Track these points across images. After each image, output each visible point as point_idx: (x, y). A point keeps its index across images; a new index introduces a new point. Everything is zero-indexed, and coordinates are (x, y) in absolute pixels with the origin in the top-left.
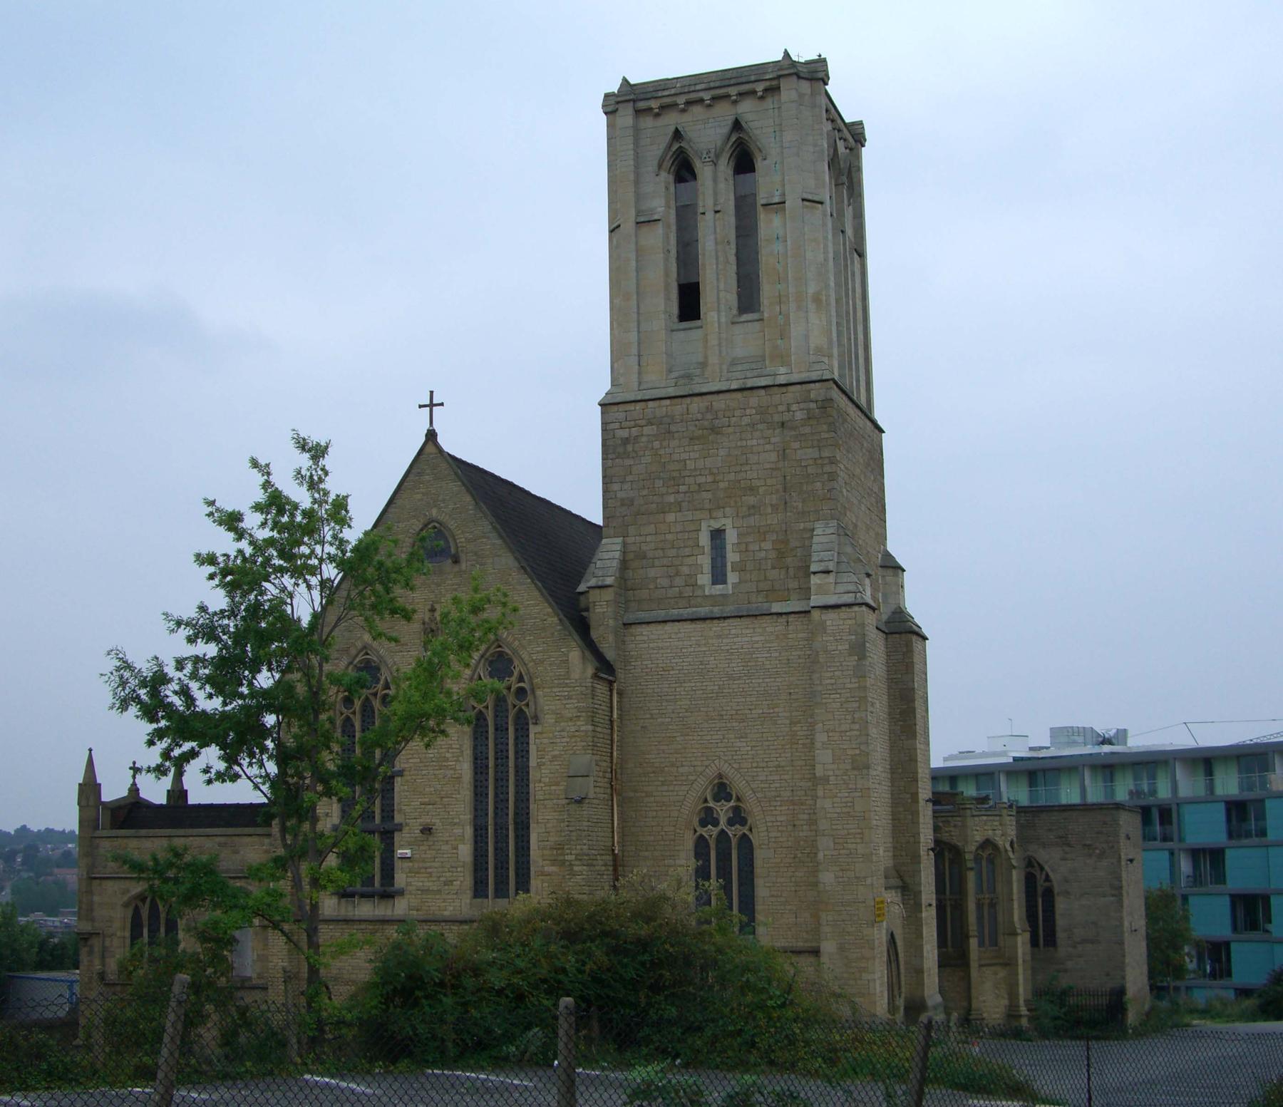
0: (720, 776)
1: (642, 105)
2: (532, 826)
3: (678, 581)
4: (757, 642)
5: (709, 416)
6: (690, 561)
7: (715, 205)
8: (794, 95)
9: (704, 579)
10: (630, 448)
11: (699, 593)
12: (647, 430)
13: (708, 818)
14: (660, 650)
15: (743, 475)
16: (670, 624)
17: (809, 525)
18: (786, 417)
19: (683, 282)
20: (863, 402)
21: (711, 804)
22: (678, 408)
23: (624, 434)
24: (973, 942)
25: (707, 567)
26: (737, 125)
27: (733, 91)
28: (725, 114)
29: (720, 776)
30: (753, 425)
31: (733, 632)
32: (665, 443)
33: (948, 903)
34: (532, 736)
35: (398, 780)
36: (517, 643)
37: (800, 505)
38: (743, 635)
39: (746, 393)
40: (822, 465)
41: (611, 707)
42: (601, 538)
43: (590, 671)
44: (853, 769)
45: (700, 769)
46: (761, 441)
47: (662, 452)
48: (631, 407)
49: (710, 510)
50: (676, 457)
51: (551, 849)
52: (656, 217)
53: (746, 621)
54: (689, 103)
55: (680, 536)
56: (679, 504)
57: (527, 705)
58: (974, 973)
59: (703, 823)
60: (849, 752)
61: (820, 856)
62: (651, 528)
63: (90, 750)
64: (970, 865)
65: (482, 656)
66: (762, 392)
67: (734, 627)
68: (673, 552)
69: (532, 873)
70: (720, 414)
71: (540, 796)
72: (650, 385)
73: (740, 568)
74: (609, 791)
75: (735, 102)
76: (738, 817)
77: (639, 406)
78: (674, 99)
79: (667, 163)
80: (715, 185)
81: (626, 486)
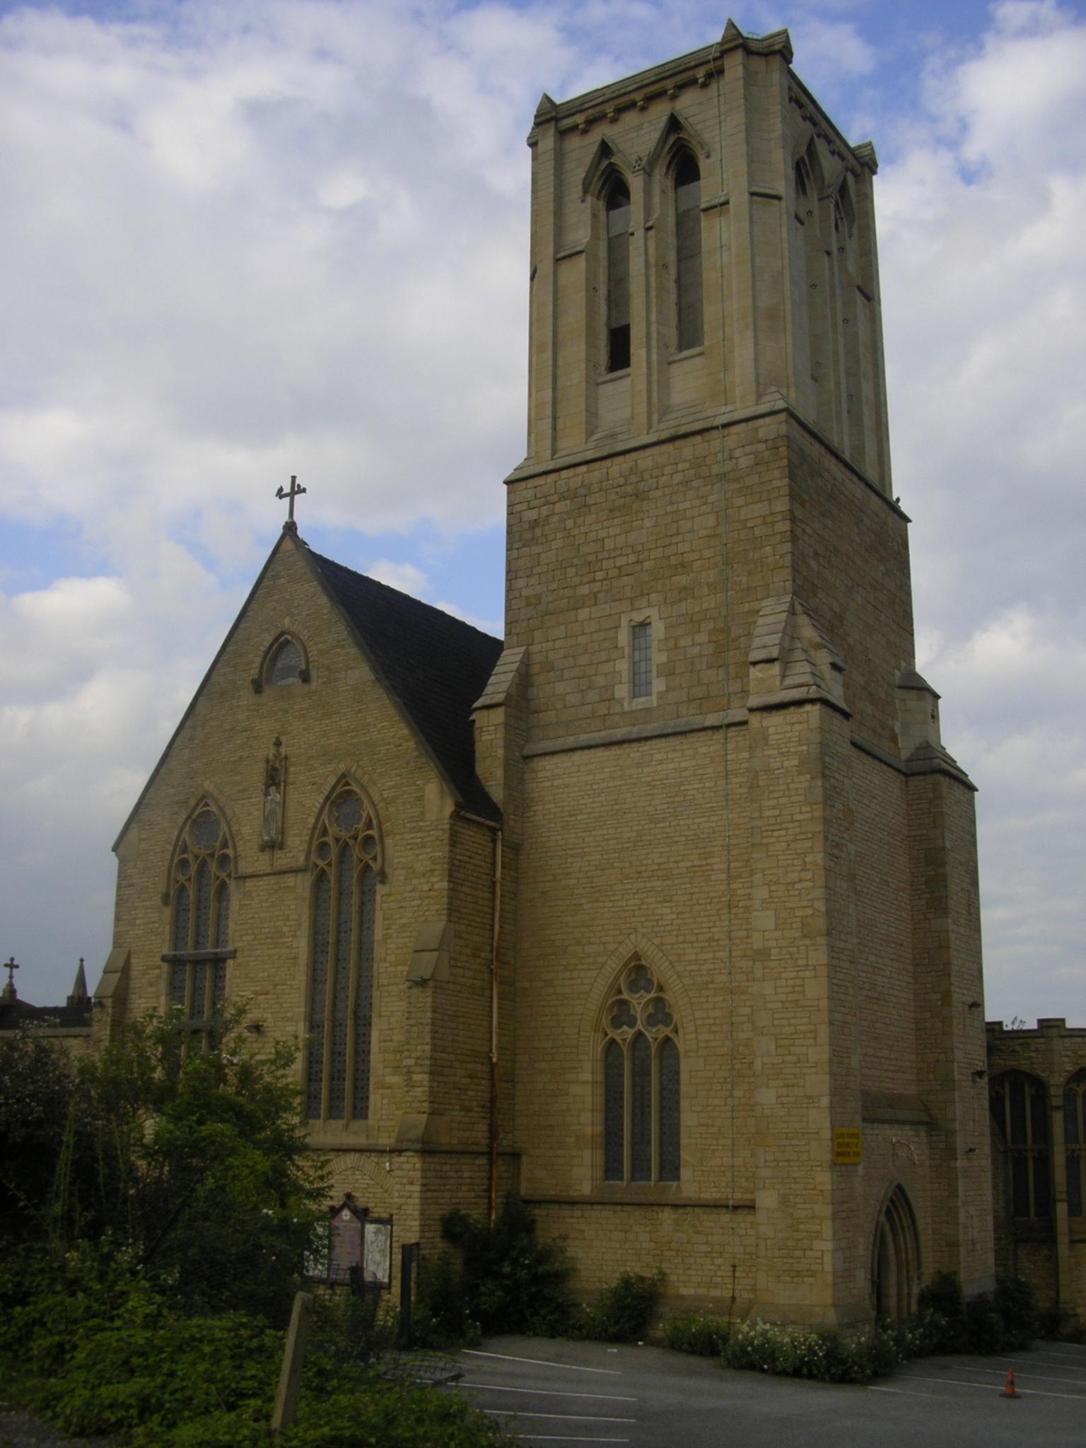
0: (636, 956)
1: (566, 123)
2: (374, 1020)
3: (592, 696)
4: (686, 769)
5: (633, 479)
6: (607, 668)
7: (646, 220)
8: (740, 71)
9: (622, 691)
10: (538, 532)
11: (617, 709)
12: (559, 507)
13: (620, 1013)
14: (575, 797)
15: (674, 548)
16: (578, 753)
17: (755, 605)
18: (729, 465)
19: (614, 326)
20: (872, 474)
21: (625, 996)
22: (597, 472)
23: (531, 515)
24: (1062, 1209)
25: (625, 676)
26: (674, 124)
27: (669, 84)
28: (659, 113)
29: (636, 956)
30: (686, 483)
31: (656, 757)
32: (580, 521)
33: (1030, 1155)
34: (378, 898)
35: (230, 963)
36: (366, 778)
37: (744, 579)
38: (664, 760)
39: (678, 443)
40: (773, 523)
41: (494, 864)
42: (502, 650)
43: (449, 807)
44: (804, 936)
45: (612, 947)
46: (697, 502)
47: (575, 532)
48: (541, 481)
49: (631, 599)
50: (592, 536)
51: (395, 1051)
52: (579, 249)
53: (672, 741)
54: (620, 110)
55: (595, 637)
56: (595, 595)
57: (375, 858)
58: (1063, 1250)
59: (616, 1023)
60: (799, 913)
61: (758, 1064)
62: (560, 632)
63: (82, 960)
64: (1057, 1102)
65: (327, 798)
66: (698, 439)
67: (657, 750)
68: (584, 660)
69: (371, 1087)
70: (647, 475)
71: (384, 981)
72: (567, 452)
73: (668, 671)
74: (486, 977)
75: (674, 98)
76: (661, 1012)
77: (551, 478)
78: (598, 109)
79: (596, 185)
80: (648, 197)
81: (533, 581)
